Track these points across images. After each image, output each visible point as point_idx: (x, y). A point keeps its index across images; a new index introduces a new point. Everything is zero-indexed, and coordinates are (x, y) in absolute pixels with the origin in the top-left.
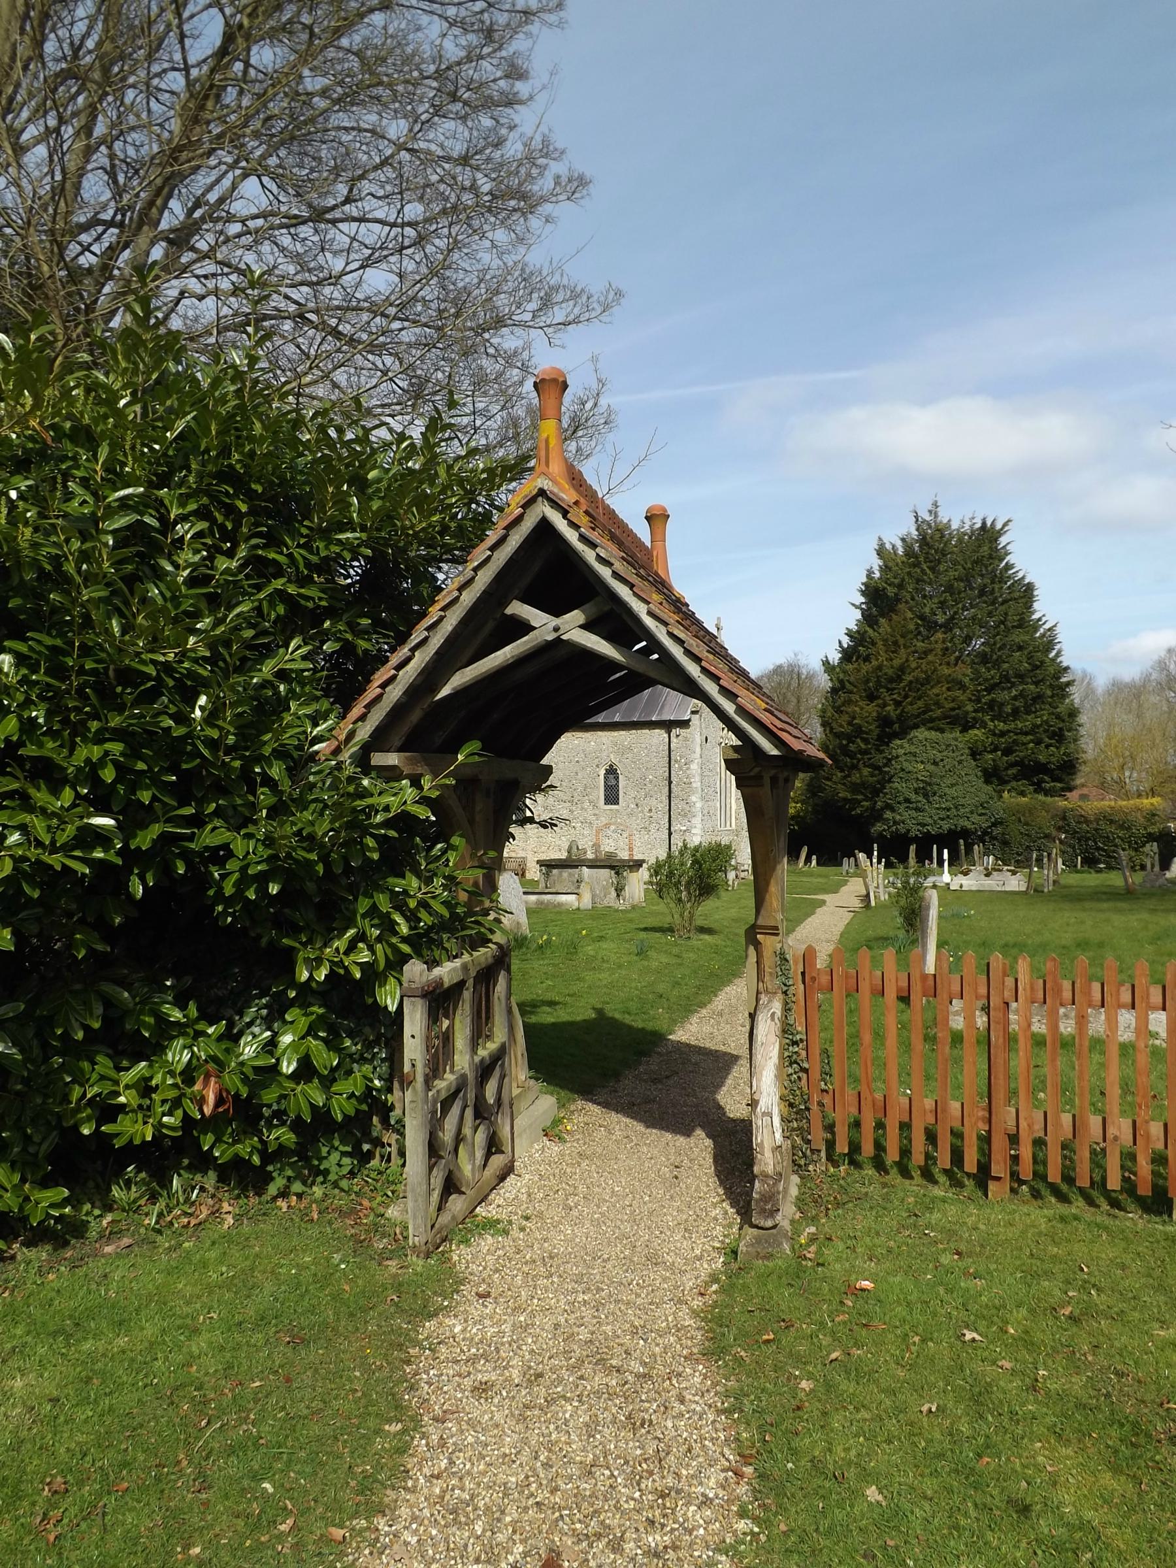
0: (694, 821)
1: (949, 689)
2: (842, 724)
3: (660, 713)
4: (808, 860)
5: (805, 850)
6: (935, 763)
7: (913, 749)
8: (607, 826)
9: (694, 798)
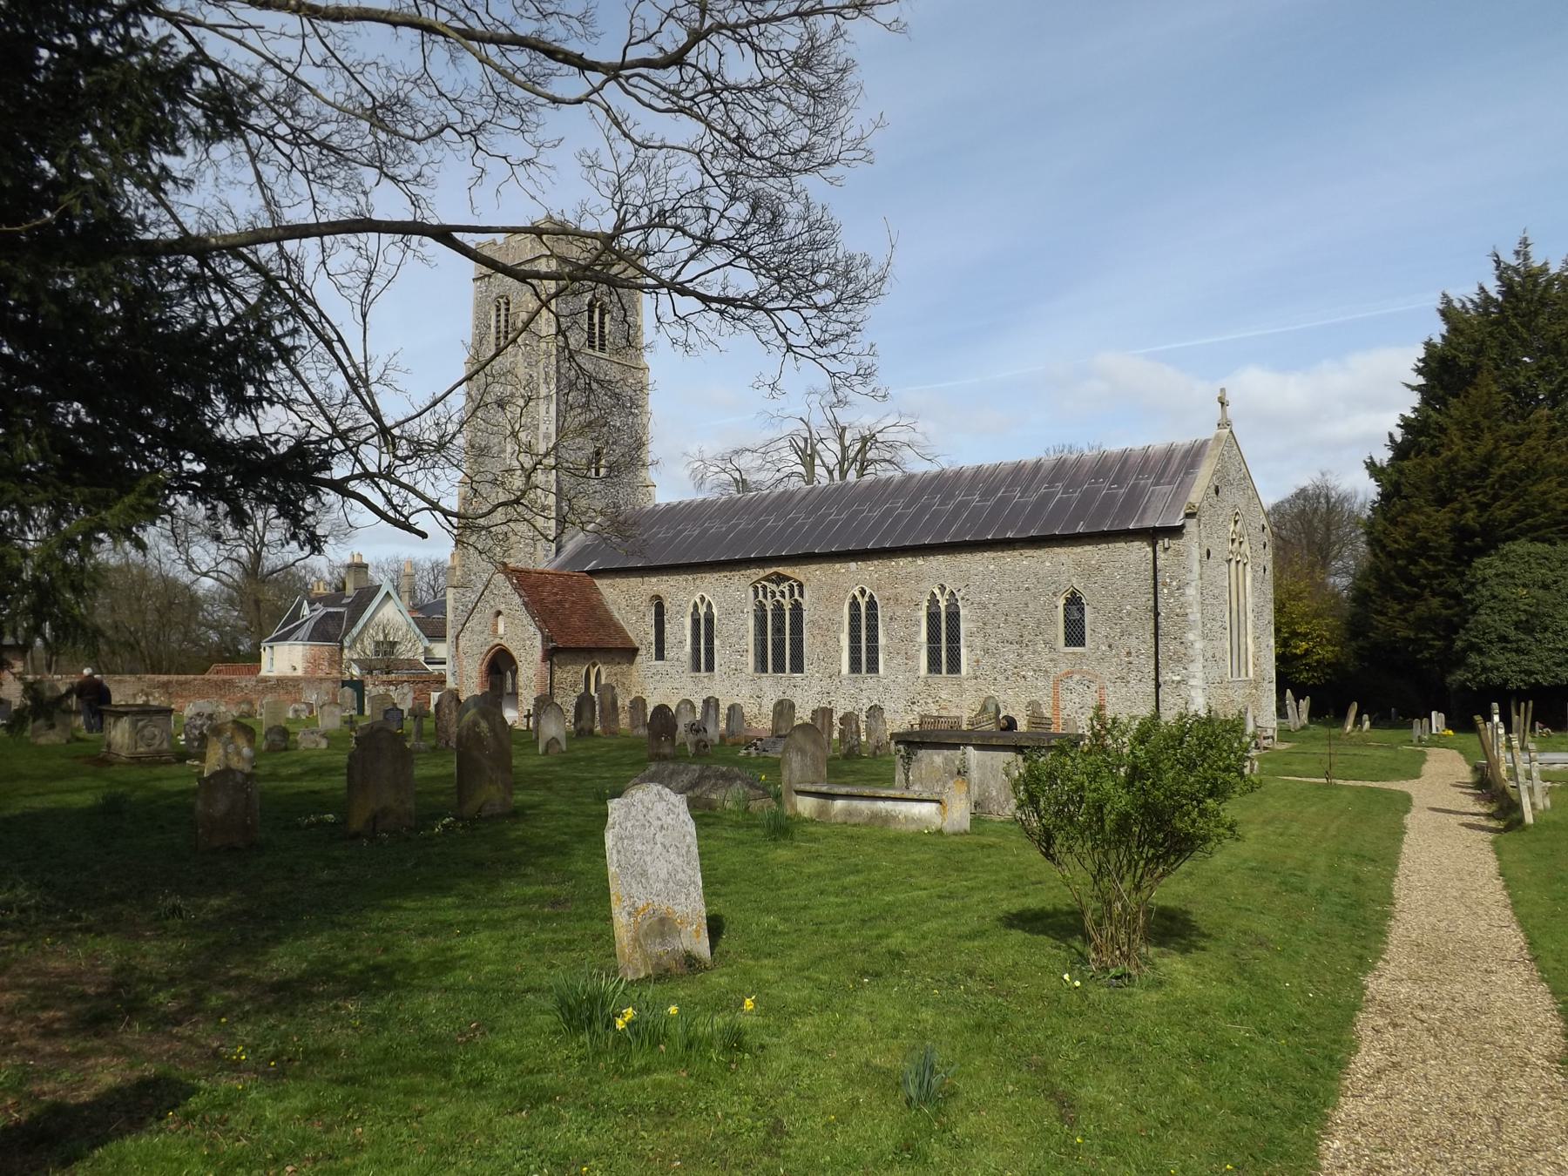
0: (1192, 667)
1: (1560, 484)
2: (1398, 539)
3: (1141, 519)
4: (1358, 721)
5: (1354, 707)
6: (1545, 587)
7: (1509, 568)
8: (1069, 675)
9: (1191, 636)
